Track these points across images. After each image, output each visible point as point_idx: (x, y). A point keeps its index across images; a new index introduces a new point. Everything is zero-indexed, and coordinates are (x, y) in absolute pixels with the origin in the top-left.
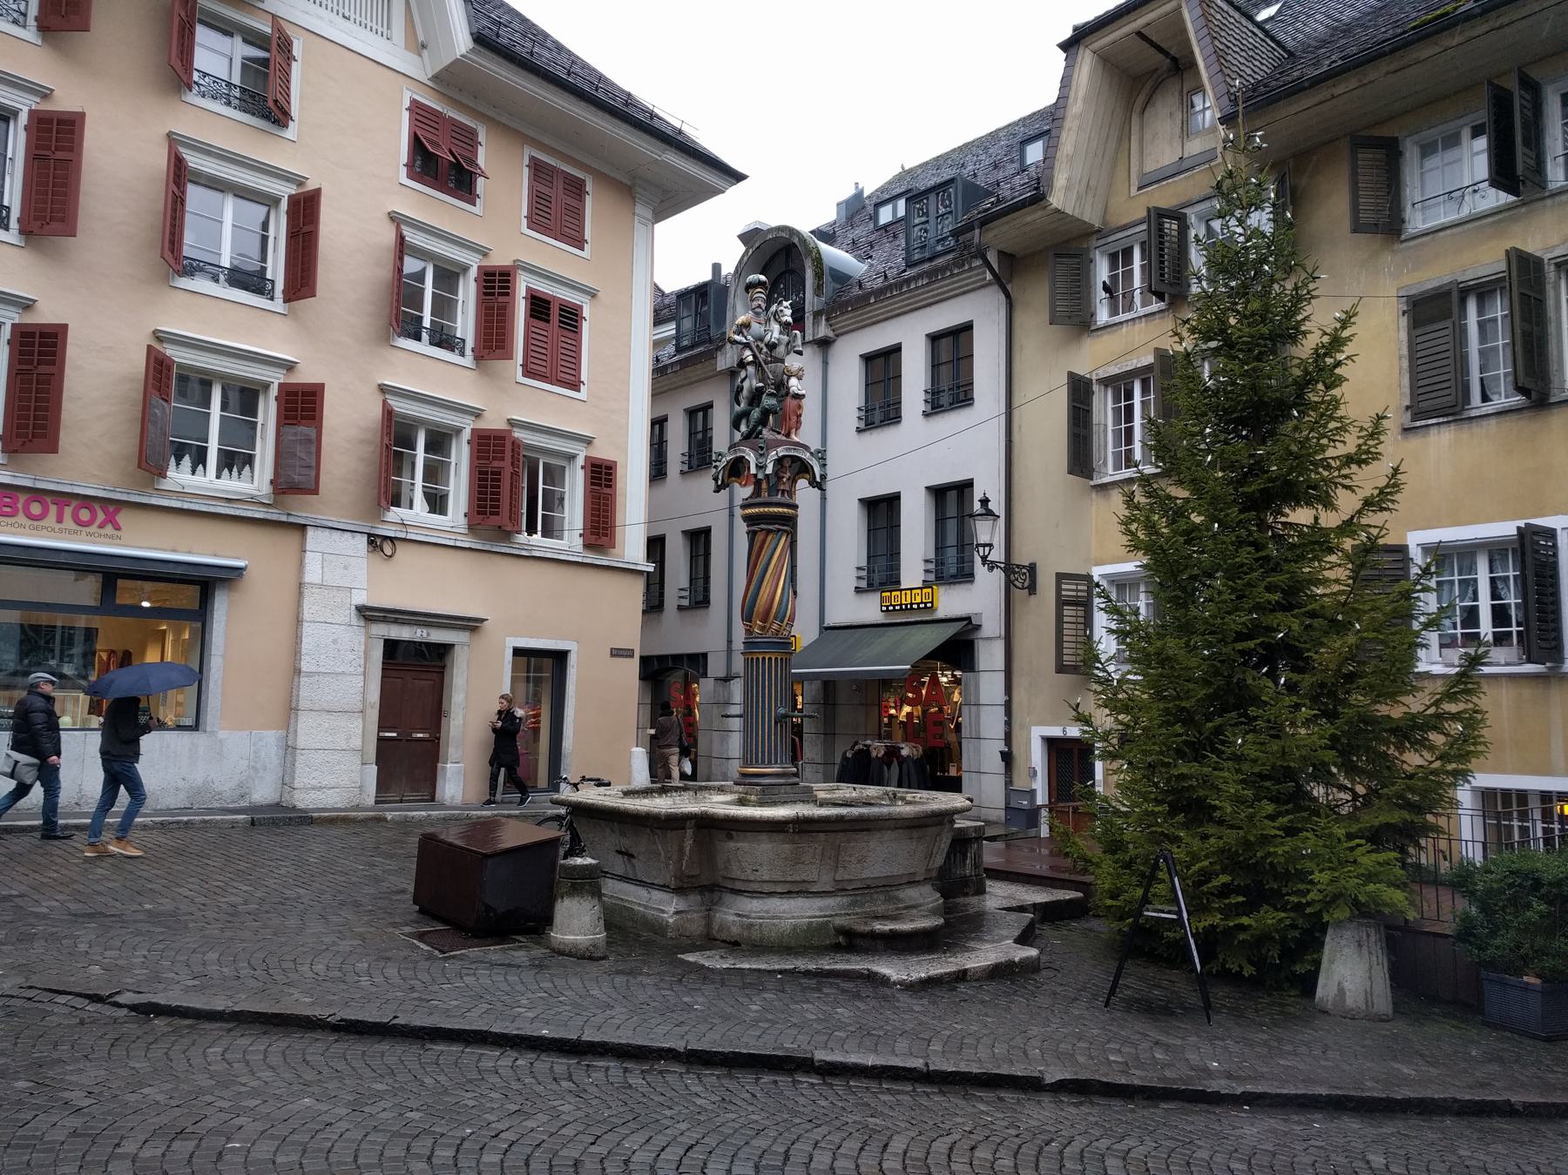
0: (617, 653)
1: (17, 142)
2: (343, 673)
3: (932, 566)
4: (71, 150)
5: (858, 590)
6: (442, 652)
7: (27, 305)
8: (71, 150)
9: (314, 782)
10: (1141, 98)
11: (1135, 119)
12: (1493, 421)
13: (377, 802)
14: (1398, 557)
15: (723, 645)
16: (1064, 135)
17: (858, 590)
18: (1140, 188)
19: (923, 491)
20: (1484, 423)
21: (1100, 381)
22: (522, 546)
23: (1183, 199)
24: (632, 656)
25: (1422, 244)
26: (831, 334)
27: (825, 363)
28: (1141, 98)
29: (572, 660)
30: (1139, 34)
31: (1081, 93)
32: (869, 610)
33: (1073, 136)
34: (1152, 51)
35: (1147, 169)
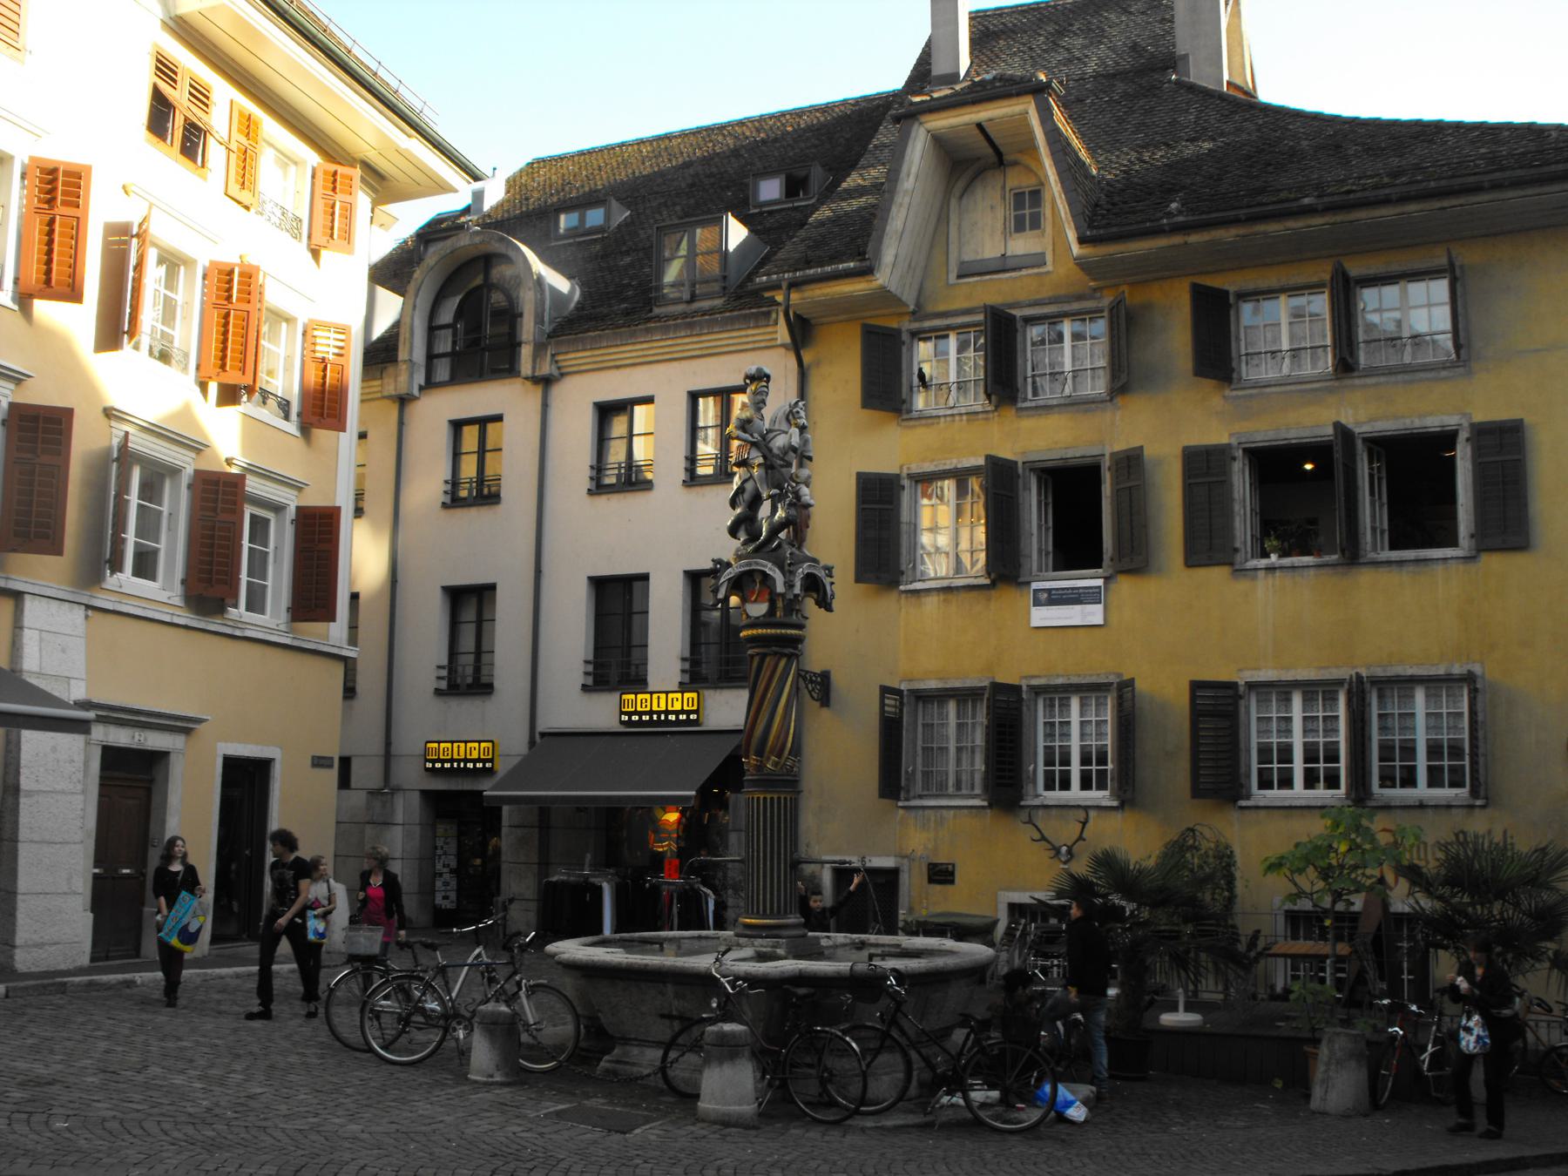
0: (320, 762)
1: (16, 196)
2: (63, 792)
3: (590, 668)
4: (891, 503)
5: (585, 688)
6: (154, 761)
7: (17, 379)
8: (891, 503)
9: (36, 938)
10: (960, 185)
11: (953, 202)
12: (1312, 572)
13: (93, 960)
14: (1230, 692)
15: (377, 747)
16: (894, 209)
17: (585, 688)
18: (959, 277)
19: (681, 575)
20: (1306, 572)
21: (910, 476)
22: (238, 624)
23: (1010, 299)
24: (331, 766)
25: (1251, 396)
26: (556, 373)
27: (545, 406)
28: (960, 185)
29: (277, 772)
30: (979, 126)
31: (914, 170)
32: (602, 713)
33: (904, 211)
34: (985, 143)
35: (966, 258)
